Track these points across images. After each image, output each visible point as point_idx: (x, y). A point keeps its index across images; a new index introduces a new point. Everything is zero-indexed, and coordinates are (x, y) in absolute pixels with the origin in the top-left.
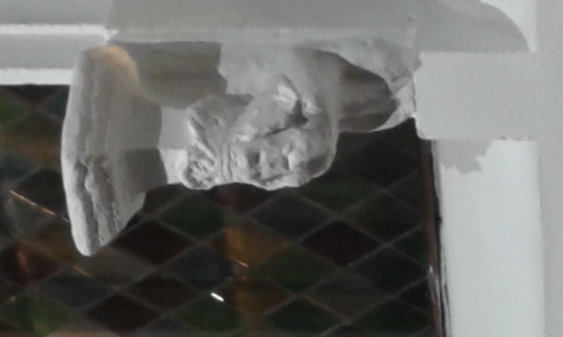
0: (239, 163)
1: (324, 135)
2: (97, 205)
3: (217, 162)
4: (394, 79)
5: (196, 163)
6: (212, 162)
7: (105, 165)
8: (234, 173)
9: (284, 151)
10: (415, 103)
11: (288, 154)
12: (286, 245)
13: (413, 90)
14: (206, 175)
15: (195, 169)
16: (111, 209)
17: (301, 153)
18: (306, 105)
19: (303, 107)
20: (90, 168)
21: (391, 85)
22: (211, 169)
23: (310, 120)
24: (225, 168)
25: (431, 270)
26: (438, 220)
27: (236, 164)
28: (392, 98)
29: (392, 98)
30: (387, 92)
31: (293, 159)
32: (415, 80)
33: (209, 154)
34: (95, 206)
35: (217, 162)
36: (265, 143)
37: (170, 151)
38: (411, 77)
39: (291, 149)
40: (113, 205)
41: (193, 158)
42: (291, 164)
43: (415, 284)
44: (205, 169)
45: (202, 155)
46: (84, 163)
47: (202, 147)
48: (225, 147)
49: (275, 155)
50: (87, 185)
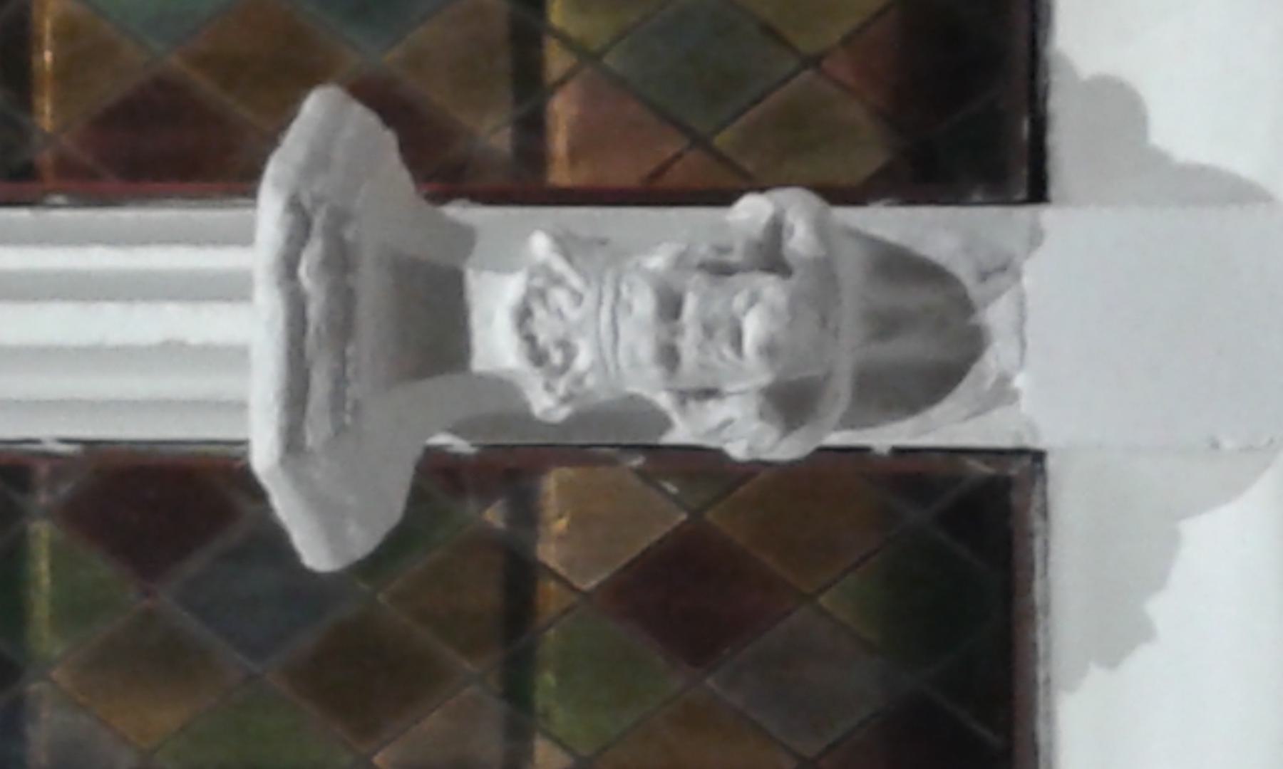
2: (318, 330)
4: (984, 276)
6: (578, 298)
7: (349, 234)
9: (739, 302)
10: (1023, 344)
11: (745, 313)
13: (1021, 304)
14: (560, 332)
15: (540, 313)
16: (343, 360)
17: (773, 312)
18: (791, 232)
19: (785, 234)
20: (318, 221)
21: (975, 290)
22: (573, 314)
23: (799, 273)
24: (605, 316)
27: (629, 308)
28: (973, 321)
29: (973, 321)
30: (966, 307)
31: (754, 327)
32: (1027, 281)
33: (575, 281)
34: (311, 330)
35: (590, 297)
36: (697, 279)
37: (487, 276)
38: (1018, 276)
39: (753, 300)
41: (538, 282)
44: (560, 313)
45: (558, 281)
46: (307, 203)
47: (559, 266)
48: (609, 277)
49: (716, 307)
50: (302, 271)
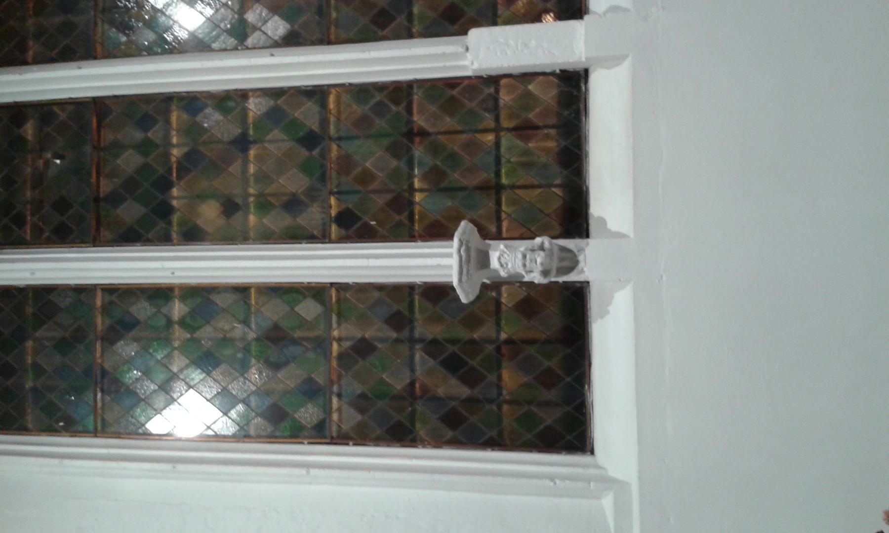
0: (519, 256)
1: (551, 259)
3: (510, 255)
4: (579, 251)
5: (502, 255)
6: (509, 255)
7: (469, 245)
8: (517, 261)
9: (536, 256)
10: (585, 263)
12: (526, 379)
13: (585, 256)
14: (505, 261)
15: (502, 258)
25: (586, 387)
26: (590, 365)
30: (575, 256)
32: (586, 252)
33: (508, 252)
40: (470, 265)
41: (502, 253)
42: (538, 263)
43: (578, 401)
45: (505, 252)
